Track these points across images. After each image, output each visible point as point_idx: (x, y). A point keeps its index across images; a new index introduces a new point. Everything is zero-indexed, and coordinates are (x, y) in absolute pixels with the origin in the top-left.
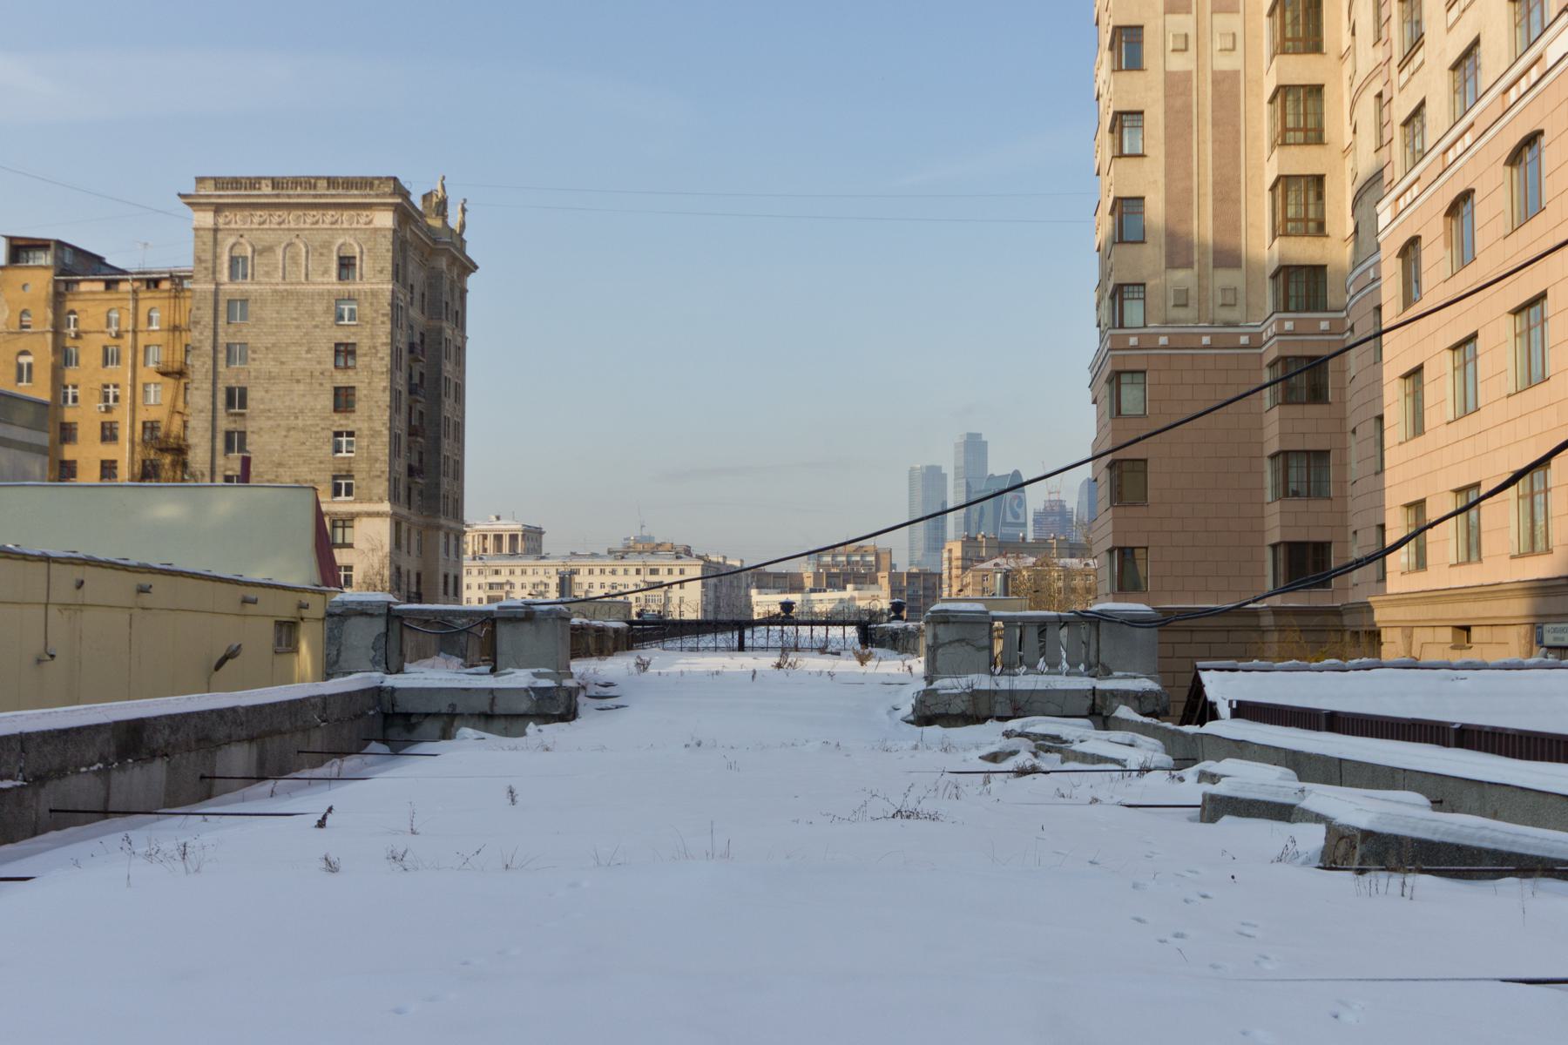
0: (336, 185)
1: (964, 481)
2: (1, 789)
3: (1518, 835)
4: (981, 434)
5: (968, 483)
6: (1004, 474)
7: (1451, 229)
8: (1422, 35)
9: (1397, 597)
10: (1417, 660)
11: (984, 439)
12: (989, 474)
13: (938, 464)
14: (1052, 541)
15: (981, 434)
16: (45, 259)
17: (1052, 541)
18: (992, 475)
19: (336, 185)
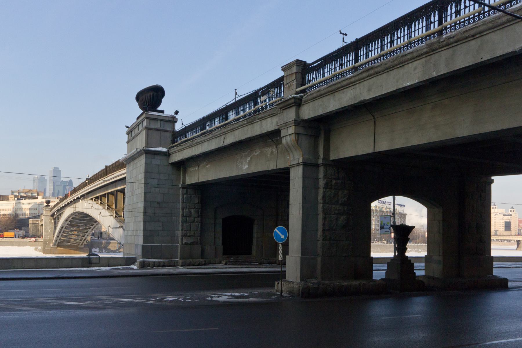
0: (289, 150)
1: (53, 182)
2: (466, 1)
3: (241, 268)
4: (59, 168)
5: (54, 183)
6: (67, 180)
7: (247, 93)
8: (128, 142)
9: (506, 25)
10: (208, 159)
11: (60, 169)
12: (61, 180)
13: (494, 182)
14: (516, 213)
15: (59, 168)
16: (59, 199)
17: (516, 213)
18: (62, 181)
19: (289, 150)
